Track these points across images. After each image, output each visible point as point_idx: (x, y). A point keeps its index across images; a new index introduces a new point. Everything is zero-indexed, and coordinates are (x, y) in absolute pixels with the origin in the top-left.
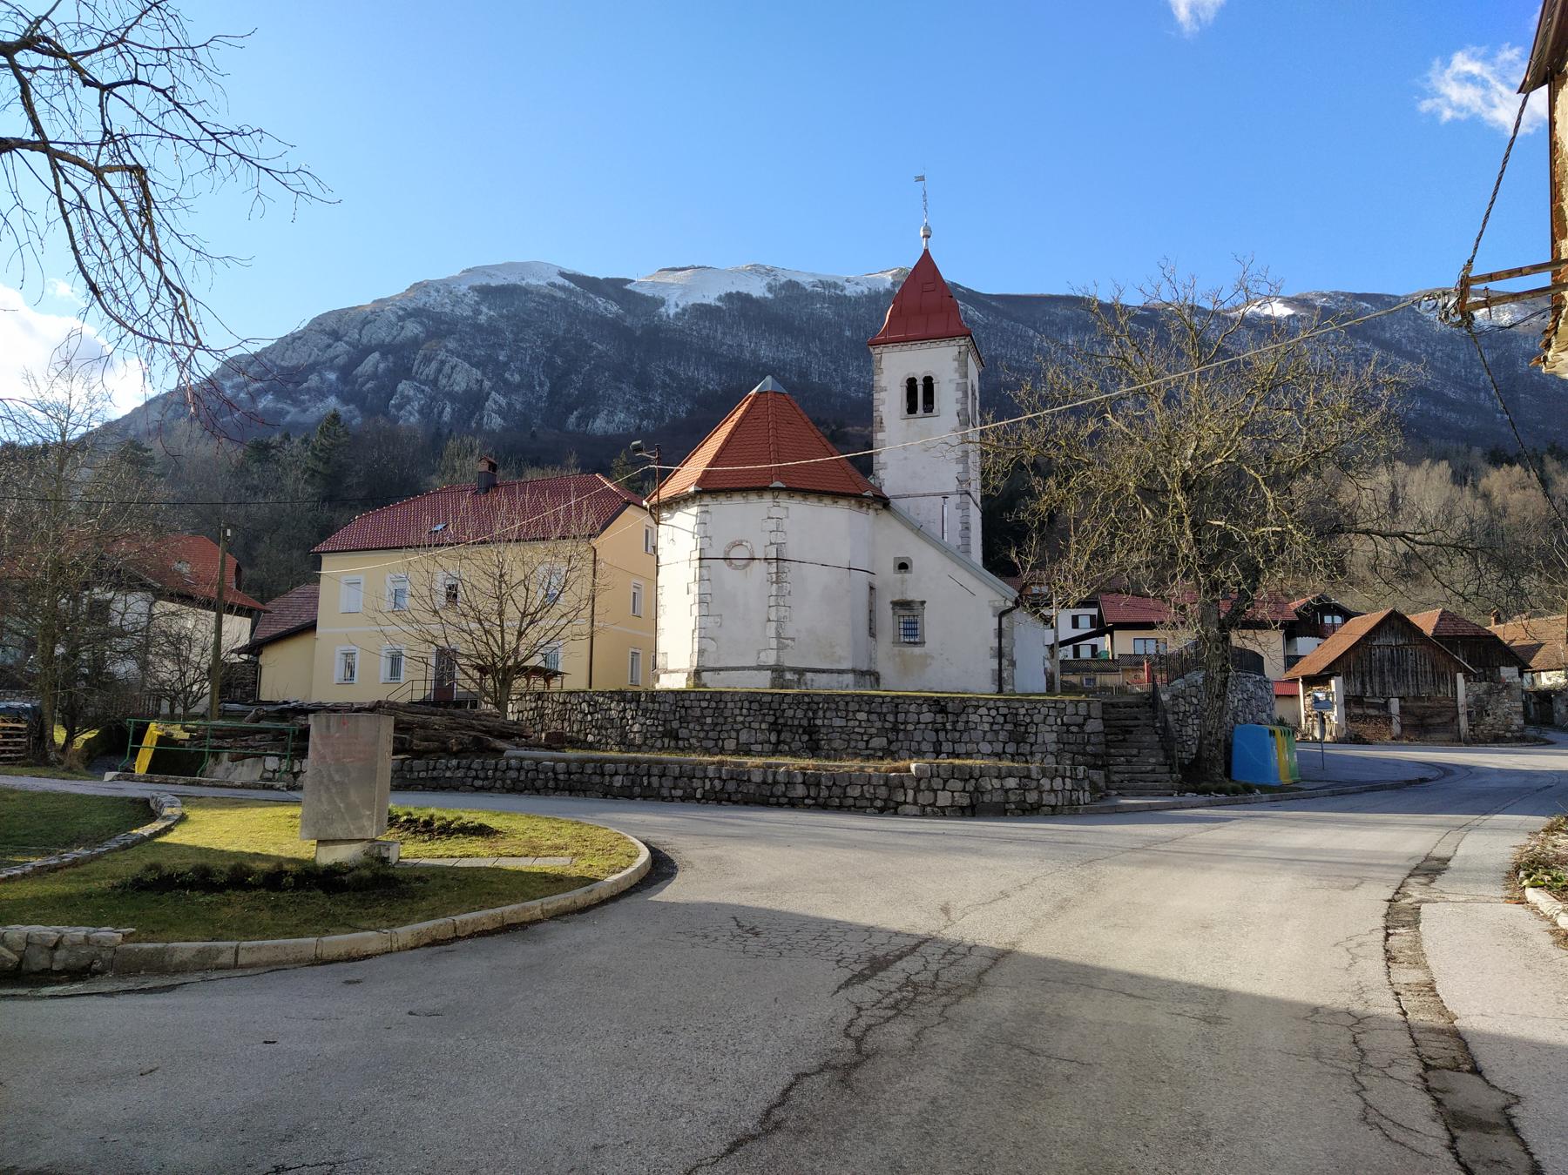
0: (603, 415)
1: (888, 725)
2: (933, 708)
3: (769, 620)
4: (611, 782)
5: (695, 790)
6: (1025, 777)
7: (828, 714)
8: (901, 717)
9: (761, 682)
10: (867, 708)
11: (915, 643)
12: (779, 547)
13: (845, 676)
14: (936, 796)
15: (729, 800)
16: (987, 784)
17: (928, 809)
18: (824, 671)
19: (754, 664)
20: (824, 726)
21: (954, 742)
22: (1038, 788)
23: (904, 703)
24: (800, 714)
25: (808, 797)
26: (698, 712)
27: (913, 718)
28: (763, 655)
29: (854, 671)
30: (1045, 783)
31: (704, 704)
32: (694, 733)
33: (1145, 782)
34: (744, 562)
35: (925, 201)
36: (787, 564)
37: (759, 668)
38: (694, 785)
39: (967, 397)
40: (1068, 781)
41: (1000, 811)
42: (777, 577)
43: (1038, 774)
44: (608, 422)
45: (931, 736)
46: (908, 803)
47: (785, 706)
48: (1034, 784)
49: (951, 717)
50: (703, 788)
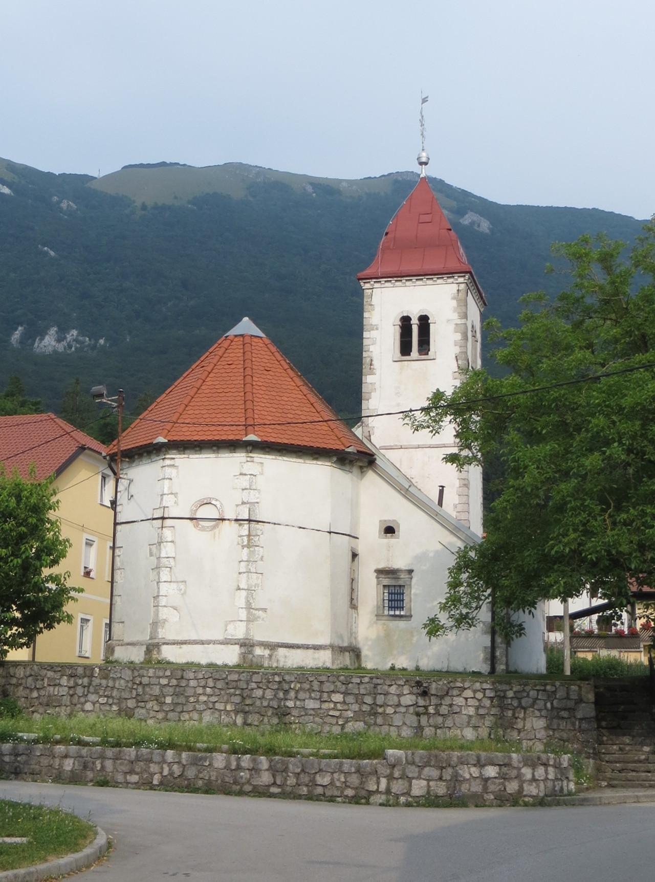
0: (53, 331)
1: (365, 708)
2: (415, 690)
3: (239, 589)
4: (61, 765)
5: (152, 775)
6: (505, 765)
7: (301, 695)
8: (380, 700)
9: (230, 656)
10: (343, 689)
11: (401, 616)
12: (252, 505)
13: (322, 652)
14: (410, 785)
15: (188, 787)
16: (466, 772)
17: (402, 799)
18: (298, 647)
19: (220, 637)
20: (295, 707)
21: (437, 727)
22: (519, 777)
23: (384, 684)
24: (269, 694)
25: (274, 784)
26: (156, 691)
27: (393, 700)
28: (230, 627)
29: (332, 647)
30: (527, 772)
31: (164, 681)
32: (152, 714)
33: (637, 772)
34: (212, 523)
35: (422, 125)
36: (260, 526)
37: (226, 642)
38: (152, 769)
39: (467, 339)
40: (551, 769)
41: (481, 806)
42: (249, 541)
43: (520, 762)
44: (59, 340)
45: (412, 720)
46: (380, 792)
47: (254, 685)
48: (514, 773)
49: (434, 701)
50: (161, 773)
